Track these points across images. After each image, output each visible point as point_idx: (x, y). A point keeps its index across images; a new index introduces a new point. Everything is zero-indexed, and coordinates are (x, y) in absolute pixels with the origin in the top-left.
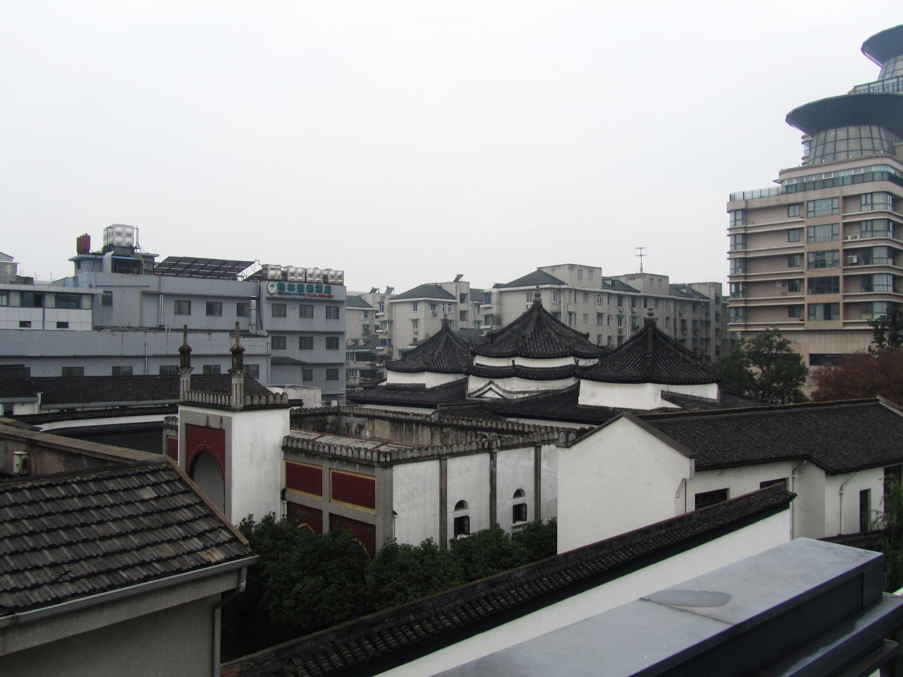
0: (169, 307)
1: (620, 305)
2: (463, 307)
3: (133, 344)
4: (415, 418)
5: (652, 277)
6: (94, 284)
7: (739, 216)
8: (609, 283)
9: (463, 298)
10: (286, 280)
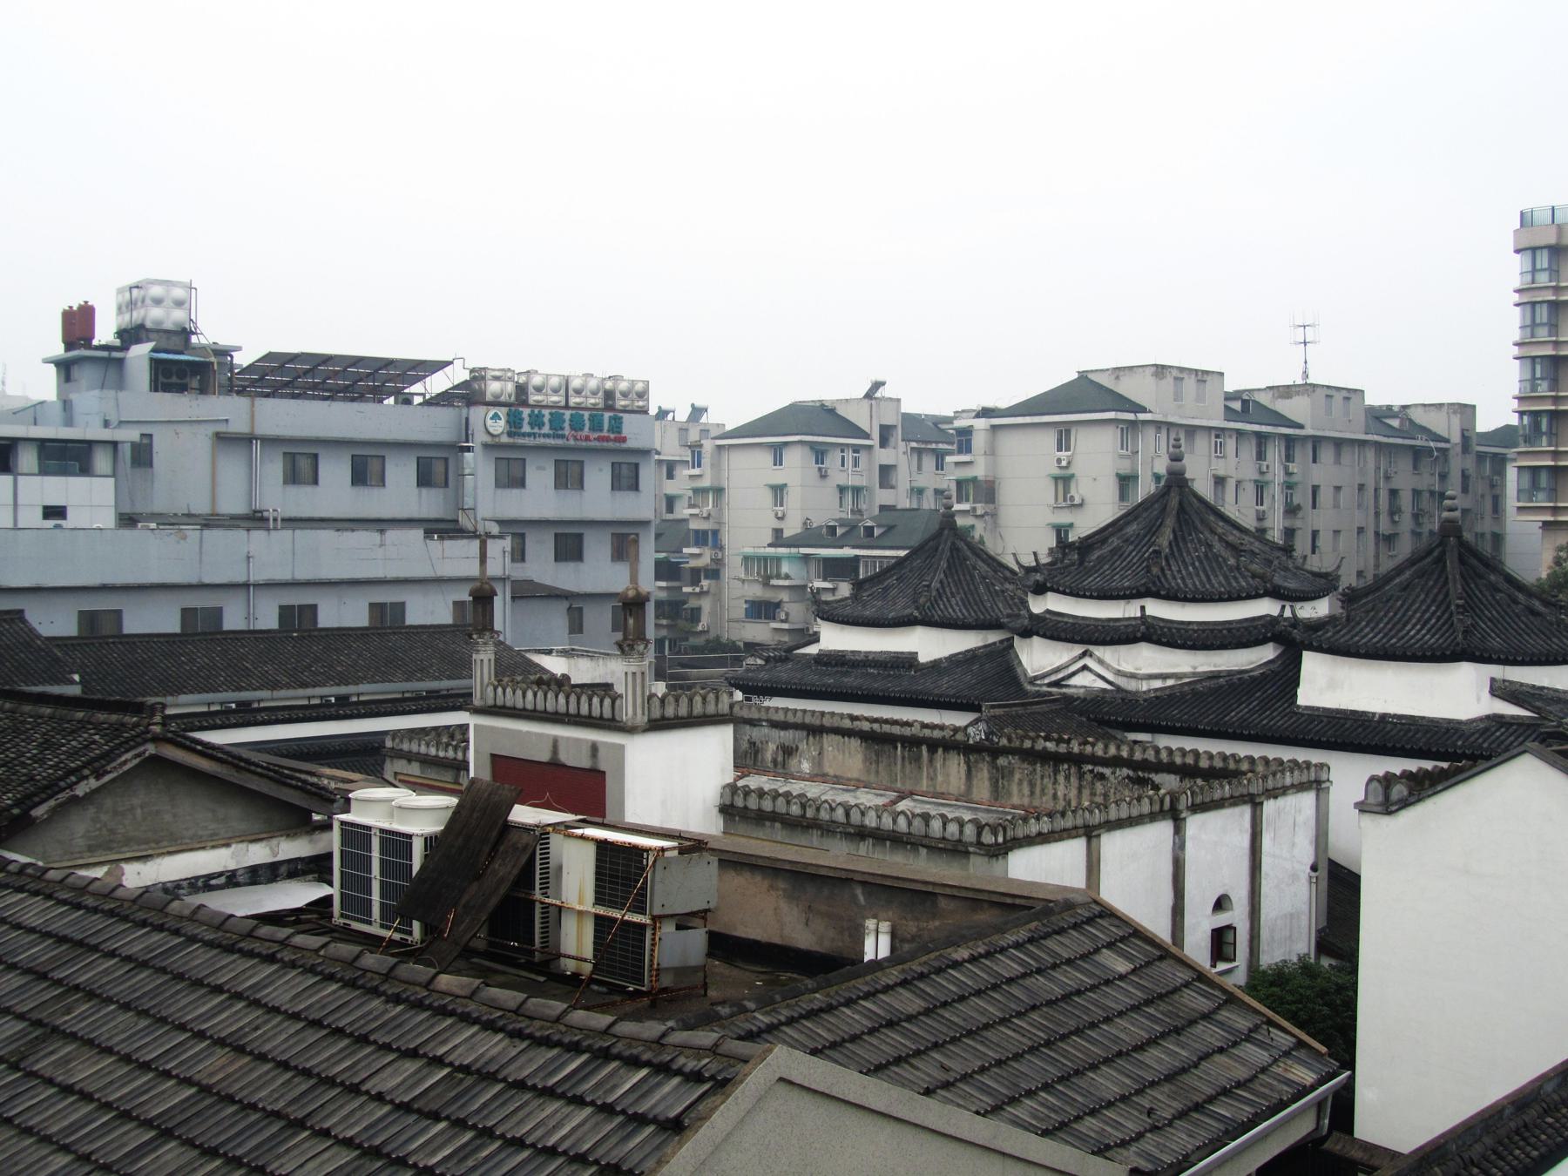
0: (273, 468)
1: (1261, 456)
2: (885, 456)
3: (223, 556)
5: (1330, 391)
6: (114, 419)
7: (1543, 260)
8: (1237, 406)
9: (886, 433)
10: (525, 404)
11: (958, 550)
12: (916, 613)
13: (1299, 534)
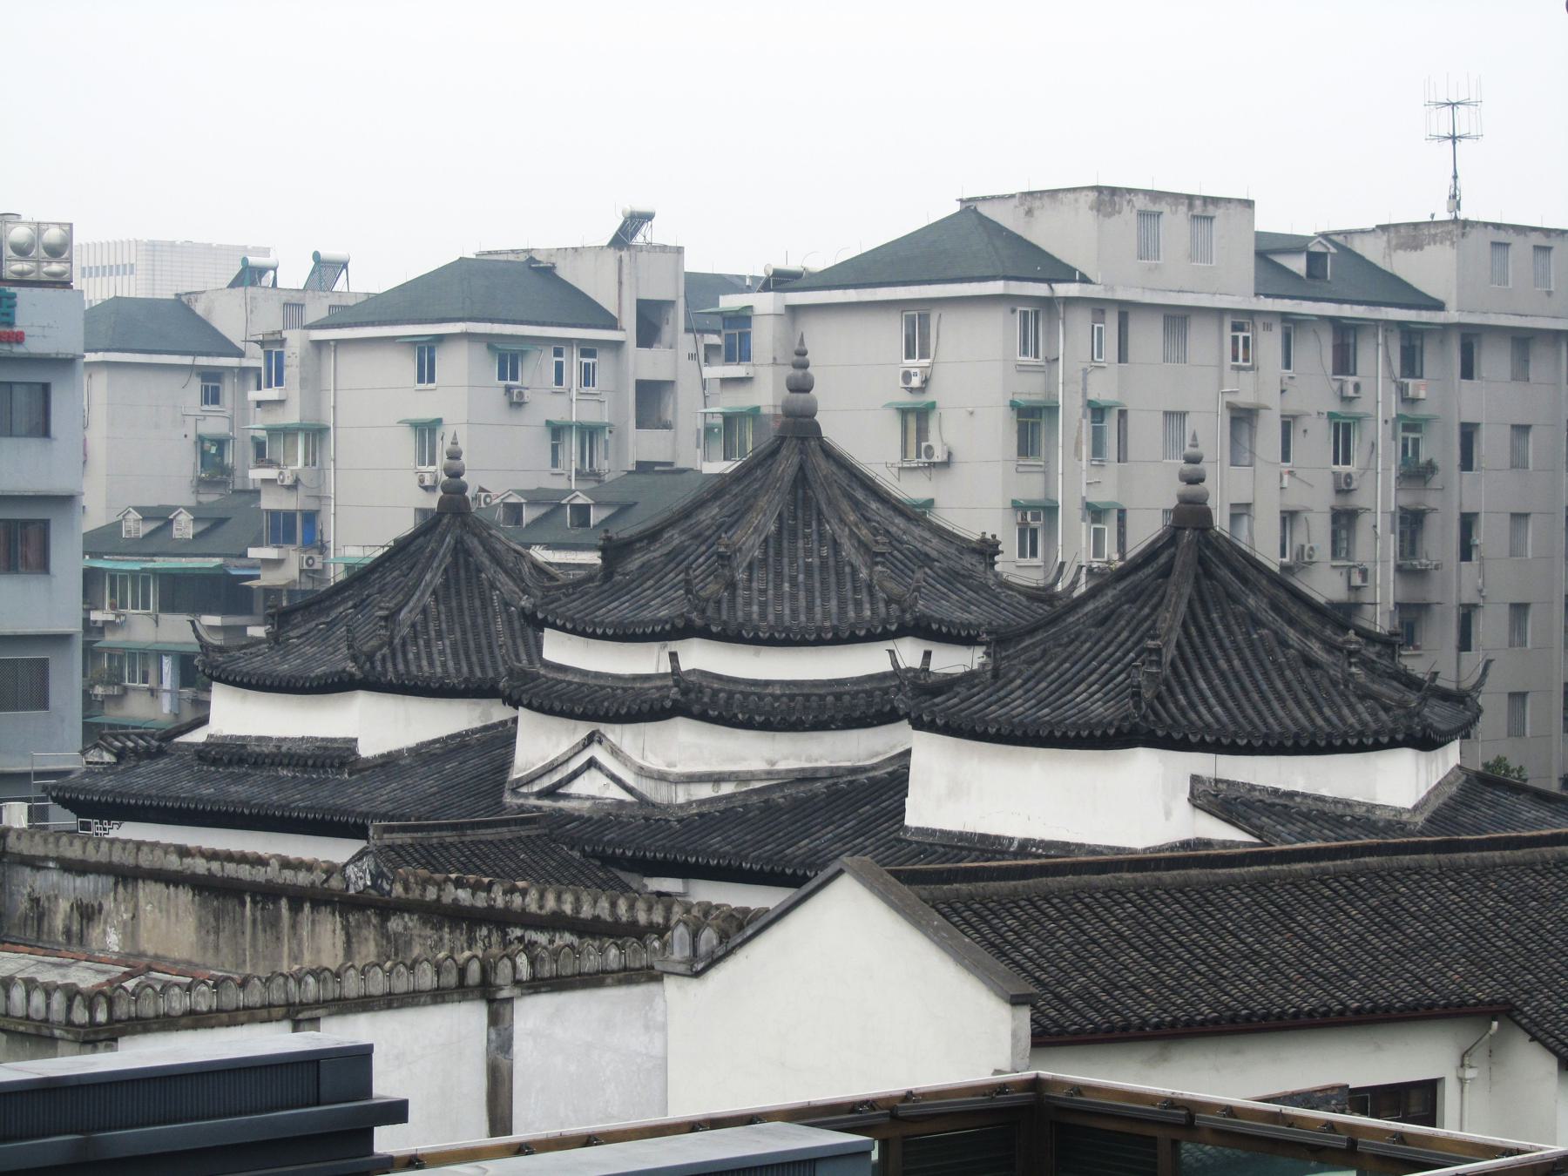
1: (1344, 363)
2: (649, 364)
4: (288, 875)
5: (1503, 236)
8: (1298, 265)
11: (468, 553)
12: (351, 667)
13: (1433, 523)
